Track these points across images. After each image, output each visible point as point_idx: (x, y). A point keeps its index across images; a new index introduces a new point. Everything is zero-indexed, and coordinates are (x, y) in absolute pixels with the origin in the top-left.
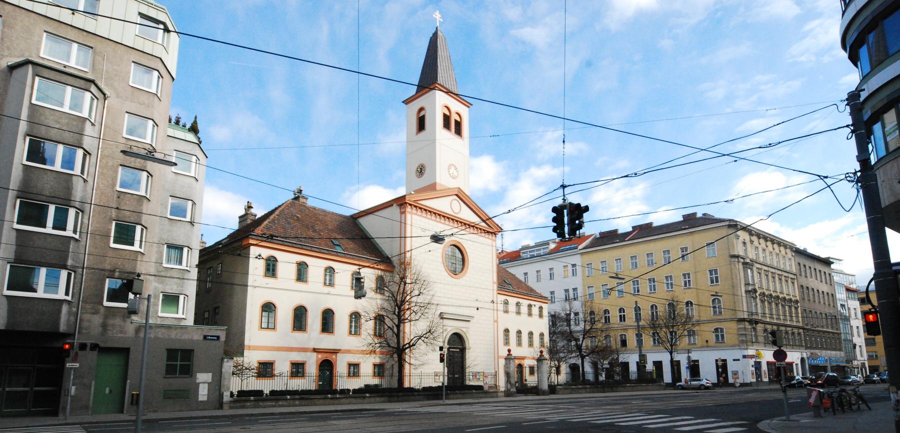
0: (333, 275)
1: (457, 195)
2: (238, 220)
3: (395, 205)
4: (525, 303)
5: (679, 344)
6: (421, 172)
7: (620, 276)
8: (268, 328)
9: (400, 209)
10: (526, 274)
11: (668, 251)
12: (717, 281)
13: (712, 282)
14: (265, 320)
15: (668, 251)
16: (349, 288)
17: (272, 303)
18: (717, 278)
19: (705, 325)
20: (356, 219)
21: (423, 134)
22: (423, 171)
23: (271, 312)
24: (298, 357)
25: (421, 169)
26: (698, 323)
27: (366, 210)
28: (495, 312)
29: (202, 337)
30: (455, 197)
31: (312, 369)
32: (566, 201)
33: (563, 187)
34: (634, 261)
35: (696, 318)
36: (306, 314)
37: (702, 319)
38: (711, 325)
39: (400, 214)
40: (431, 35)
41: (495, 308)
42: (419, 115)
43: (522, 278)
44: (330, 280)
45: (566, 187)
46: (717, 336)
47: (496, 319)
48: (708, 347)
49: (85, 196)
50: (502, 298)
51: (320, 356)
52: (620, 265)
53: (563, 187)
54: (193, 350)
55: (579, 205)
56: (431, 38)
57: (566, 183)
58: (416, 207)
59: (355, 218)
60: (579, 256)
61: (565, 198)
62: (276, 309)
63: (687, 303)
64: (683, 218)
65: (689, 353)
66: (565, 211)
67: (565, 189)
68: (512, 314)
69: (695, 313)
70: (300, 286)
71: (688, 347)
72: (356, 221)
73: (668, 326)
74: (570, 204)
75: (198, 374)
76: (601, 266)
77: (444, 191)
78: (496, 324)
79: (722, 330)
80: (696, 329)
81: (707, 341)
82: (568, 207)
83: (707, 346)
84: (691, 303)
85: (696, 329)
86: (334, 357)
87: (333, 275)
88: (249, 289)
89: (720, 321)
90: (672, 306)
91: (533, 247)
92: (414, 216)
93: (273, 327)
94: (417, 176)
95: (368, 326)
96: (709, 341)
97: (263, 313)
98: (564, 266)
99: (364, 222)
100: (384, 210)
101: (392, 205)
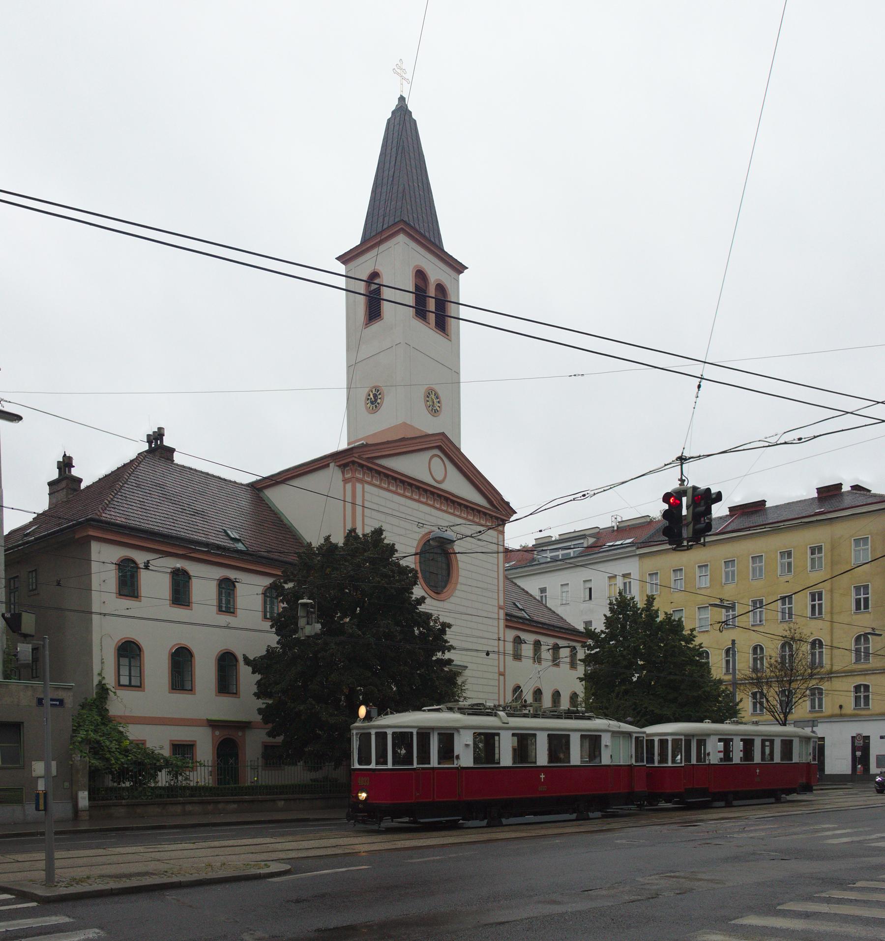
0: (231, 592)
1: (439, 448)
2: (47, 489)
3: (332, 465)
4: (547, 642)
5: (795, 712)
6: (376, 400)
7: (877, 632)
8: (130, 685)
9: (343, 473)
10: (543, 590)
11: (789, 554)
12: (866, 607)
13: (858, 607)
14: (125, 671)
15: (789, 554)
16: (260, 615)
17: (133, 642)
18: (866, 600)
19: (840, 679)
20: (260, 490)
21: (376, 327)
22: (379, 401)
23: (133, 658)
24: (182, 734)
25: (375, 396)
26: (831, 675)
27: (273, 476)
28: (502, 657)
29: (35, 701)
30: (437, 452)
31: (205, 752)
32: (686, 483)
33: (682, 459)
34: (730, 569)
35: (827, 667)
36: (191, 661)
37: (835, 668)
38: (850, 679)
39: (342, 483)
40: (389, 116)
41: (501, 650)
42: (368, 289)
43: (536, 594)
44: (228, 602)
45: (686, 459)
46: (857, 699)
47: (502, 670)
48: (841, 715)
49: (801, 637)
50: (511, 634)
51: (217, 733)
52: (820, 605)
53: (682, 459)
54: (23, 723)
55: (708, 490)
56: (389, 120)
57: (687, 454)
58: (370, 469)
59: (259, 488)
60: (637, 558)
61: (684, 478)
62: (142, 653)
63: (813, 643)
64: (818, 492)
65: (813, 726)
66: (684, 499)
67: (680, 455)
68: (527, 662)
69: (826, 660)
70: (179, 613)
71: (810, 716)
72: (261, 495)
73: (783, 681)
74: (695, 488)
75: (33, 763)
76: (673, 578)
77: (418, 441)
78: (502, 678)
79: (867, 687)
80: (825, 686)
81: (841, 707)
82: (690, 492)
83: (840, 716)
84: (820, 643)
85: (825, 686)
86: (240, 734)
87: (231, 592)
88: (95, 617)
89: (864, 673)
90: (788, 643)
91: (557, 542)
92: (367, 487)
93: (139, 685)
94: (368, 409)
95: (247, 679)
96: (844, 706)
97: (121, 659)
98: (610, 578)
99: (277, 497)
100: (313, 474)
101: (327, 466)
